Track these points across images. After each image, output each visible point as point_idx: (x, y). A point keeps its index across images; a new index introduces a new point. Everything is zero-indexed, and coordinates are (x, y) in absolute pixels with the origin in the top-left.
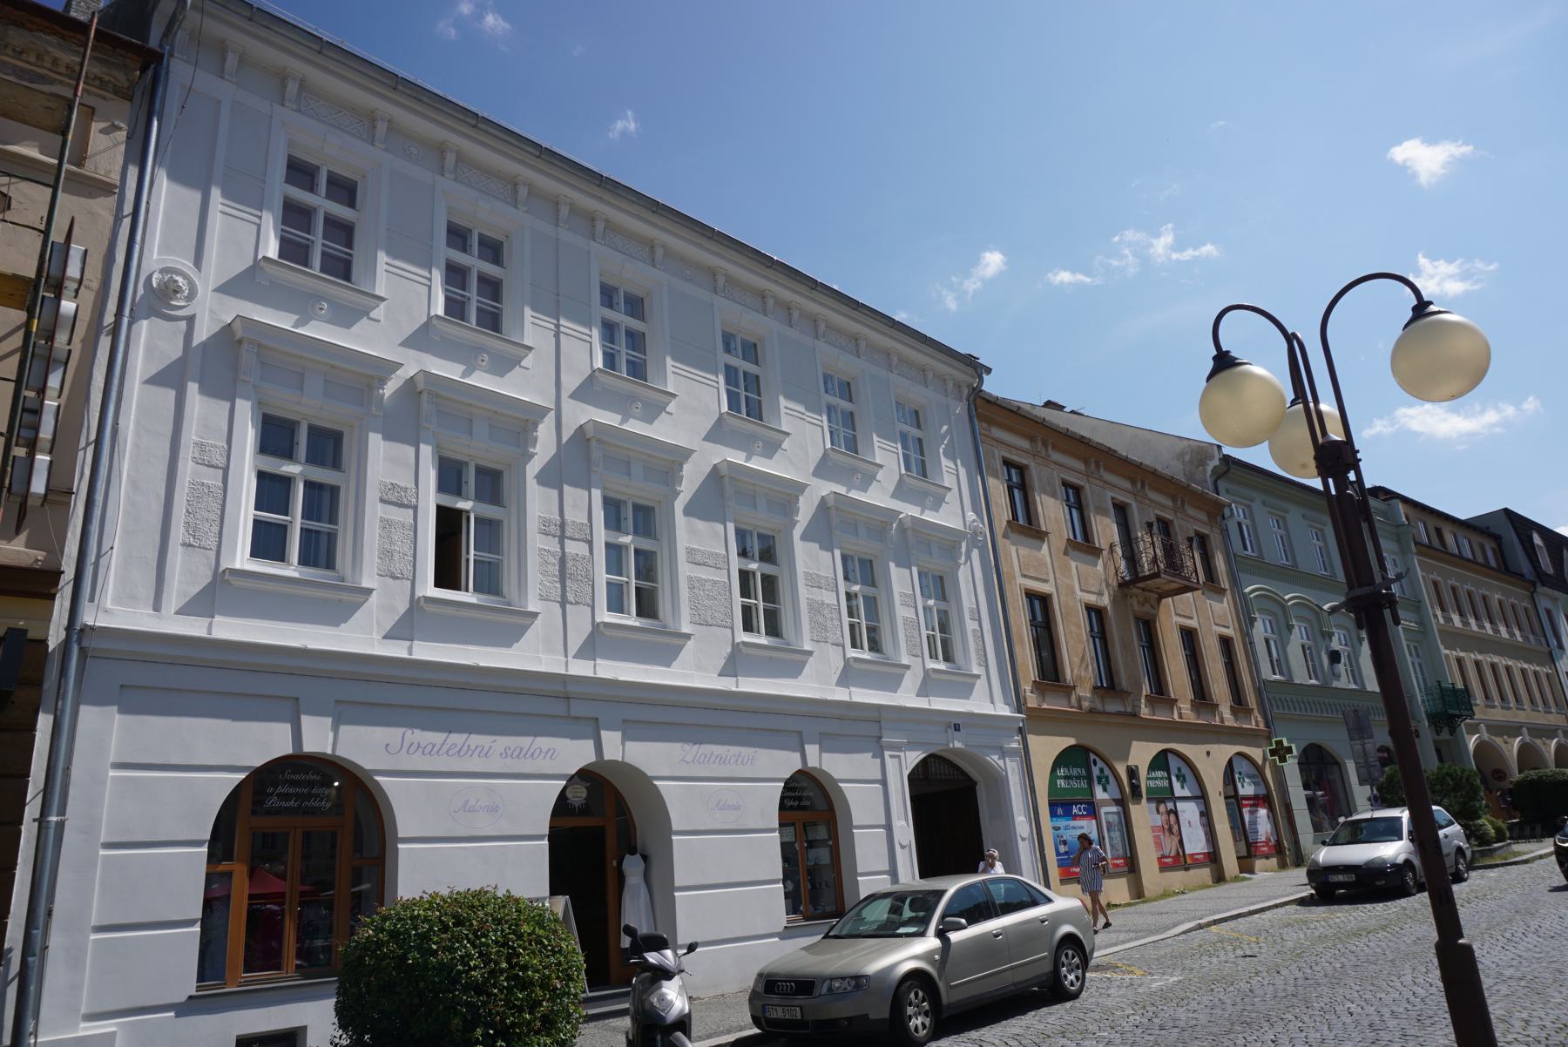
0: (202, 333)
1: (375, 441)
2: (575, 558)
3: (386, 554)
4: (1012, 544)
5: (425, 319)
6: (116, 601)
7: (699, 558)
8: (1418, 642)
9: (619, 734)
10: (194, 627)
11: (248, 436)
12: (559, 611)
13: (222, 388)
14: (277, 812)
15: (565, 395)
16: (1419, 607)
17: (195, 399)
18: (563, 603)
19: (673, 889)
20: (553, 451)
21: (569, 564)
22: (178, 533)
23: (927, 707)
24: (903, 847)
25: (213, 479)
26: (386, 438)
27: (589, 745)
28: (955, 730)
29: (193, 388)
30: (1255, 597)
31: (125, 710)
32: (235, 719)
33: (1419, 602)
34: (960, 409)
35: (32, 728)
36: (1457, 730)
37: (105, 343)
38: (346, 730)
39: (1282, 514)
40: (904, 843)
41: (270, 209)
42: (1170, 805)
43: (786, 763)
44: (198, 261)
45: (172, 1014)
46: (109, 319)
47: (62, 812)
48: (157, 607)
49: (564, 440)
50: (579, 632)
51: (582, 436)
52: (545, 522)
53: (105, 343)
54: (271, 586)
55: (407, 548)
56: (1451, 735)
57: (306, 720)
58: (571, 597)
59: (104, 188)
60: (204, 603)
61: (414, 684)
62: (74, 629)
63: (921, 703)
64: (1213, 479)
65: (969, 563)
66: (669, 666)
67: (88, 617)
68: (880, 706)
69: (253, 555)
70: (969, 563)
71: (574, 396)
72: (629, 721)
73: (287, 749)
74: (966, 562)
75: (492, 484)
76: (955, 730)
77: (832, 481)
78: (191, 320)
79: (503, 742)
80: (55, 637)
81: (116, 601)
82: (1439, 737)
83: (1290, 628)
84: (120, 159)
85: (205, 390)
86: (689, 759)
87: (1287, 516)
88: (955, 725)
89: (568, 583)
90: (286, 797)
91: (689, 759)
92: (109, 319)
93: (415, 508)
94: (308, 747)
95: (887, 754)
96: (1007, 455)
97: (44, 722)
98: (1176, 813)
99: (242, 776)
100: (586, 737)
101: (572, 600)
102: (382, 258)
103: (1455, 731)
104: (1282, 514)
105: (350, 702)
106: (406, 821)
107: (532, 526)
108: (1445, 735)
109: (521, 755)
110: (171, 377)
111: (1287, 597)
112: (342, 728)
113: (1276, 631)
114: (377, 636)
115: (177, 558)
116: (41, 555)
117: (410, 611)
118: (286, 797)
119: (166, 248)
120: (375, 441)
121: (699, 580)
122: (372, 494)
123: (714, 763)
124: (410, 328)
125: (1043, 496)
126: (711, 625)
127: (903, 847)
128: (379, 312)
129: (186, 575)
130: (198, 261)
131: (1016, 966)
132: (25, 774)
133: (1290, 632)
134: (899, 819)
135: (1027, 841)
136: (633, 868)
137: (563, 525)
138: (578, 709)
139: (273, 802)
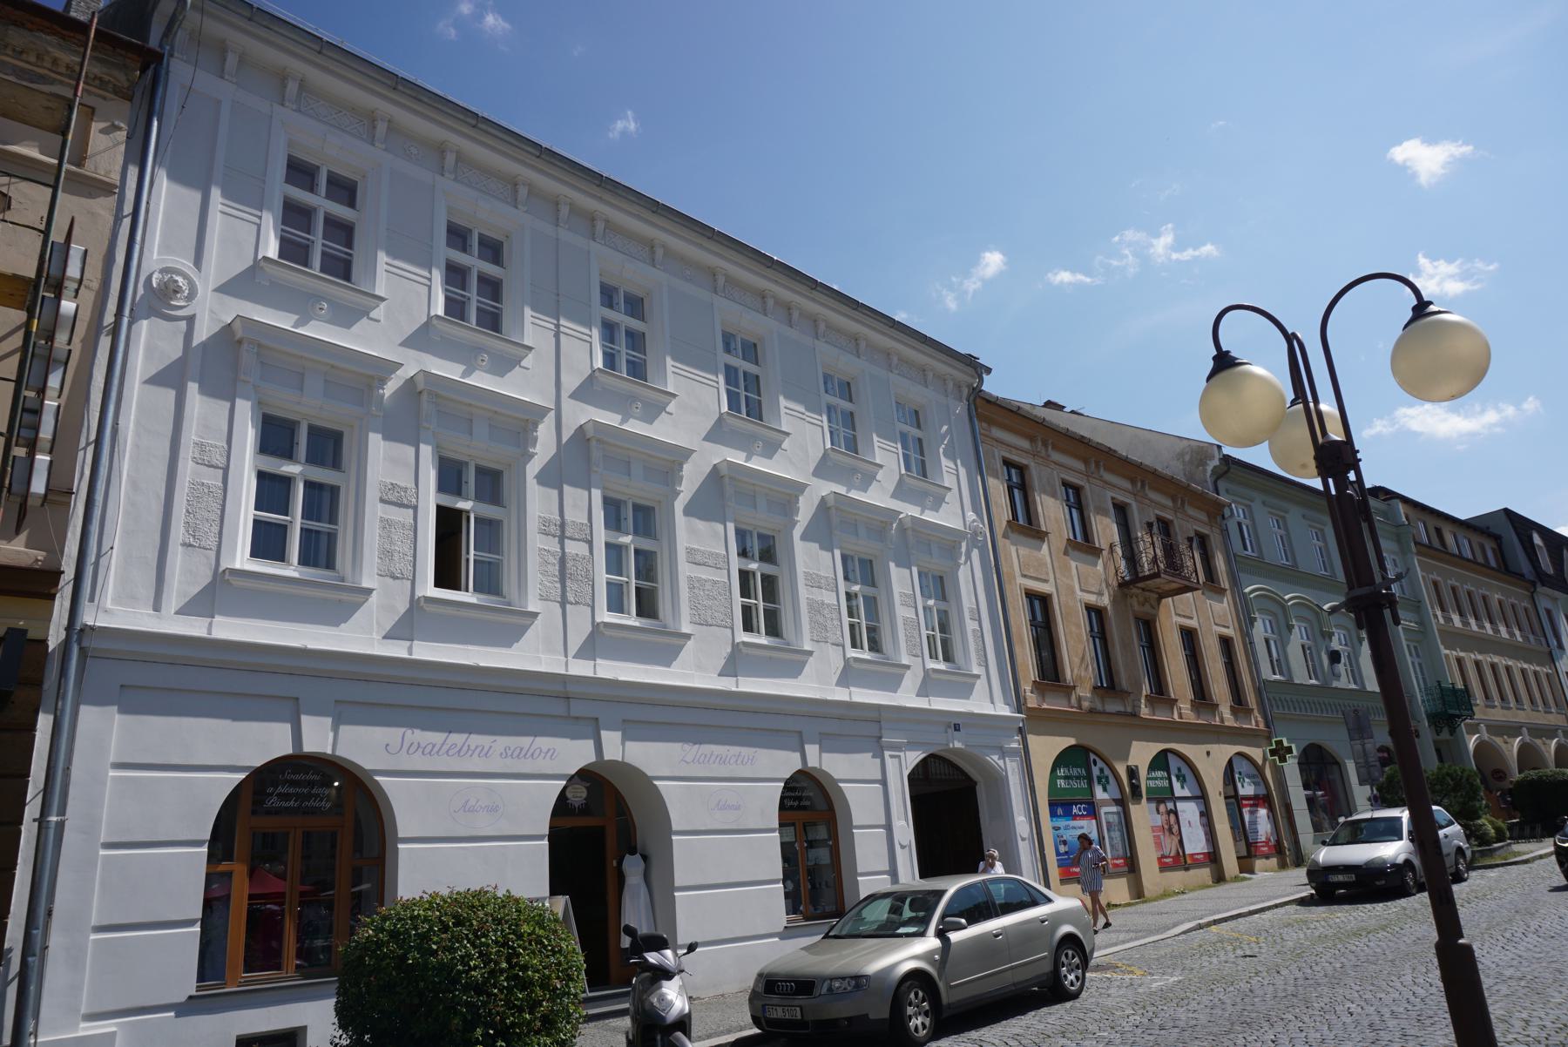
0: (202, 333)
1: (375, 441)
2: (575, 558)
3: (386, 554)
4: (1012, 544)
5: (425, 319)
6: (116, 601)
7: (699, 558)
8: (1418, 642)
9: (619, 734)
10: (194, 627)
11: (248, 436)
12: (559, 611)
13: (222, 388)
14: (277, 812)
15: (565, 395)
16: (1419, 607)
17: (195, 399)
18: (563, 603)
19: (673, 889)
20: (553, 451)
21: (569, 564)
22: (178, 533)
23: (927, 707)
24: (903, 847)
25: (213, 479)
26: (386, 438)
27: (589, 745)
28: (955, 730)
29: (193, 388)
30: (1255, 597)
31: (125, 710)
32: (235, 719)
33: (1419, 602)
34: (960, 409)
35: (32, 728)
36: (1457, 730)
37: (105, 343)
38: (346, 730)
39: (1282, 514)
40: (904, 843)
41: (270, 209)
42: (1170, 805)
43: (786, 763)
44: (198, 261)
45: (172, 1014)
46: (109, 319)
47: (62, 812)
48: (157, 607)
49: (564, 440)
50: (579, 632)
51: (582, 436)
52: (545, 522)
53: (105, 343)
54: (271, 586)
55: (407, 548)
56: (1451, 735)
57: (306, 720)
58: (571, 597)
59: (104, 188)
60: (204, 603)
61: (414, 684)
62: (74, 629)
63: (921, 703)
64: (1213, 479)
65: (969, 563)
66: (669, 666)
67: (88, 617)
68: (880, 706)
69: (253, 555)
70: (969, 563)
71: (574, 396)
72: (629, 721)
73: (287, 749)
74: (966, 562)
75: (492, 484)
76: (955, 730)
77: (832, 481)
78: (191, 320)
79: (503, 742)
80: (55, 637)
81: (116, 601)
82: (1439, 737)
83: (1290, 628)
84: (120, 159)
85: (205, 390)
86: (689, 759)
87: (1287, 516)
88: (955, 725)
89: (568, 583)
90: (286, 797)
91: (689, 759)
92: (109, 319)
93: (415, 508)
94: (308, 747)
95: (887, 754)
96: (1007, 455)
97: (44, 722)
98: (1176, 813)
99: (242, 776)
100: (586, 737)
101: (572, 600)
102: (382, 258)
103: (1455, 731)
104: (1282, 514)
105: (350, 702)
106: (406, 821)
107: (532, 526)
108: (1445, 735)
109: (521, 755)
110: (171, 377)
111: (1287, 597)
112: (342, 728)
113: (1276, 631)
114: (377, 636)
115: (177, 558)
116: (41, 555)
117: (410, 611)
118: (286, 797)
119: (166, 248)
120: (375, 441)
121: (699, 580)
122: (372, 494)
123: (714, 763)
124: (410, 328)
125: (1043, 496)
126: (711, 625)
127: (903, 847)
128: (379, 312)
129: (186, 575)
130: (198, 261)
131: (1016, 966)
132: (25, 774)
133: (1290, 632)
134: (899, 819)
135: (1027, 841)
136: (633, 868)
137: (563, 525)
138: (578, 709)
139: (273, 802)
